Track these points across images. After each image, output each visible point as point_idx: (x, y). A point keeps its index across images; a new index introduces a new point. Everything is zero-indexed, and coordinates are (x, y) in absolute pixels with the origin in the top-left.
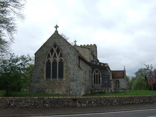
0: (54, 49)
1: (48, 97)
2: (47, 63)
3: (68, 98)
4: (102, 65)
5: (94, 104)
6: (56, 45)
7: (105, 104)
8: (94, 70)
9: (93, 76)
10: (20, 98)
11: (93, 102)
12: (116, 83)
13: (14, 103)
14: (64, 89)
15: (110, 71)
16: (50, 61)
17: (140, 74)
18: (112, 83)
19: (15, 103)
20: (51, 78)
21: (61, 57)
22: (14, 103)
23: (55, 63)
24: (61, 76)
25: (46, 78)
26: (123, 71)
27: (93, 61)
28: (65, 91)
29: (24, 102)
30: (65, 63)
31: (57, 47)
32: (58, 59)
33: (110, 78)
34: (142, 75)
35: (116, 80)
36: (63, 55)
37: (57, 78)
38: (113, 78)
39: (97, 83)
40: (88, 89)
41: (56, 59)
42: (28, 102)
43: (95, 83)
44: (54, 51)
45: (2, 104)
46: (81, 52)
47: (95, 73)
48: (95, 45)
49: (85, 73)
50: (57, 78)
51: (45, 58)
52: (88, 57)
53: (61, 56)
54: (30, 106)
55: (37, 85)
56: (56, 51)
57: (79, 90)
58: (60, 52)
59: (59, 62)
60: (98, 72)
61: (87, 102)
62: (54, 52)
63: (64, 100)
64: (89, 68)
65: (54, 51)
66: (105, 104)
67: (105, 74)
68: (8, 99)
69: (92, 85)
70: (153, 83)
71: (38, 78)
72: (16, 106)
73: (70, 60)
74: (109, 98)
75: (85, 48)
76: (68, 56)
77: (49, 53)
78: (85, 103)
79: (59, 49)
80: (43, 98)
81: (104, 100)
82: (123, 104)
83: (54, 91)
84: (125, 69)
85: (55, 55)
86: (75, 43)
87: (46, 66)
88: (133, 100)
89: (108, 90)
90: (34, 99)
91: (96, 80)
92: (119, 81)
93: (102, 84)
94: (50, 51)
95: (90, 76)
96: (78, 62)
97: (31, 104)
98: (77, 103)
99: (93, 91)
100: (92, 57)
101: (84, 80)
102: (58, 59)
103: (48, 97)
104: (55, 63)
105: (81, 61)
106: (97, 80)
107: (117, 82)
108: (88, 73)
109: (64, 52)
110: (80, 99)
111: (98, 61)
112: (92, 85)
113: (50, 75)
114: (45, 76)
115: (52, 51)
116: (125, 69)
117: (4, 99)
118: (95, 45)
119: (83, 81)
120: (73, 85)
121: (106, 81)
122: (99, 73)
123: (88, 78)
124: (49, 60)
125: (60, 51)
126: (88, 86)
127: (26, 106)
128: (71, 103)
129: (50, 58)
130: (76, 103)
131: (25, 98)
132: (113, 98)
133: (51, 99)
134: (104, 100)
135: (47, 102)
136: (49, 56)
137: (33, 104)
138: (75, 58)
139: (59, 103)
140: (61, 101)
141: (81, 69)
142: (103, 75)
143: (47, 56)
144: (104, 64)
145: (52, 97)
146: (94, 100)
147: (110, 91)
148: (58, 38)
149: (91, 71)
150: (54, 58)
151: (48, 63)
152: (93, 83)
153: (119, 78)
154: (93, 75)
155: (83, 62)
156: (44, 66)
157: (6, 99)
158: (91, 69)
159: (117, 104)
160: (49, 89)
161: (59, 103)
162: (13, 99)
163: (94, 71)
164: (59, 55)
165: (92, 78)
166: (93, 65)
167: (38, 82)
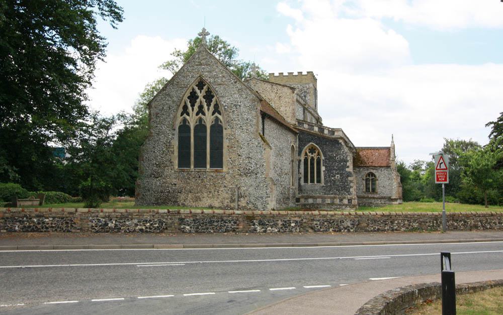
0: (198, 91)
1: (188, 210)
2: (180, 127)
3: (234, 213)
4: (44, 294)
5: (297, 229)
6: (202, 82)
7: (322, 230)
8: (305, 145)
9: (303, 161)
10: (127, 212)
11: (293, 225)
12: (367, 180)
13: (114, 222)
14: (225, 195)
15: (346, 149)
16: (187, 124)
17: (447, 157)
18: (351, 182)
19: (116, 221)
20: (192, 167)
21: (217, 114)
22: (114, 222)
23: (201, 127)
24: (217, 162)
25: (180, 165)
26: (388, 149)
28: (227, 199)
29: (136, 221)
30: (226, 129)
31: (205, 88)
32: (209, 119)
33: (348, 167)
34: (453, 161)
35: (367, 172)
36: (221, 109)
37: (208, 166)
38: (355, 166)
39: (312, 181)
40: (286, 196)
42: (146, 221)
43: (306, 181)
44: (198, 97)
45: (90, 223)
46: (269, 94)
47: (306, 154)
48: (311, 74)
49: (279, 155)
50: (208, 166)
52: (288, 110)
53: (217, 110)
54: (150, 229)
56: (204, 97)
57: (262, 198)
58: (214, 100)
59: (212, 127)
61: (280, 223)
62: (198, 100)
63: (225, 218)
64: (291, 140)
66: (322, 230)
67: (335, 157)
68: (101, 214)
69: (300, 185)
70: (446, 182)
71: (158, 166)
72: (120, 228)
73: (239, 120)
74: (332, 216)
75: (280, 85)
76: (233, 111)
77: (185, 103)
78: (276, 225)
79: (211, 92)
80: (179, 213)
81: (319, 221)
82: (366, 231)
83: (200, 199)
84: (393, 142)
85: (201, 110)
87: (179, 135)
88: (392, 222)
89: (341, 200)
90: (158, 213)
91: (310, 171)
92: (375, 176)
93: (326, 182)
94: (189, 98)
95: (293, 161)
96: (261, 126)
97: (151, 224)
98: (257, 226)
99: (302, 201)
100: (301, 110)
101: (276, 171)
102: (209, 119)
103: (188, 210)
104: (201, 127)
105: (268, 123)
106: (312, 173)
107: (371, 180)
109: (225, 101)
110: (264, 216)
111: (318, 120)
112: (300, 185)
114: (176, 162)
115: (193, 97)
116: (393, 142)
117: (93, 213)
119: (272, 174)
120: (247, 184)
121: (338, 177)
122: (319, 154)
123: (287, 167)
124: (185, 120)
125: (213, 97)
126: (289, 189)
128: (242, 224)
129: (188, 114)
130: (254, 225)
131: (139, 212)
132: (343, 216)
133: (195, 215)
134: (319, 221)
135: (188, 221)
136: (185, 110)
137: (156, 224)
138: (254, 117)
139: (215, 224)
140: (220, 220)
141: (268, 144)
142: (329, 159)
143: (181, 110)
144: (332, 131)
145: (199, 211)
146: (297, 219)
147: (345, 201)
148: (209, 65)
149: (296, 149)
150: (197, 114)
151: (184, 128)
152: (302, 180)
153: (375, 167)
154: (302, 158)
155: (274, 126)
156: (173, 135)
157: (97, 214)
159: (352, 230)
160: (188, 194)
161: (215, 224)
162: (112, 213)
163: (306, 149)
164: (212, 108)
166: (302, 132)
167: (157, 176)
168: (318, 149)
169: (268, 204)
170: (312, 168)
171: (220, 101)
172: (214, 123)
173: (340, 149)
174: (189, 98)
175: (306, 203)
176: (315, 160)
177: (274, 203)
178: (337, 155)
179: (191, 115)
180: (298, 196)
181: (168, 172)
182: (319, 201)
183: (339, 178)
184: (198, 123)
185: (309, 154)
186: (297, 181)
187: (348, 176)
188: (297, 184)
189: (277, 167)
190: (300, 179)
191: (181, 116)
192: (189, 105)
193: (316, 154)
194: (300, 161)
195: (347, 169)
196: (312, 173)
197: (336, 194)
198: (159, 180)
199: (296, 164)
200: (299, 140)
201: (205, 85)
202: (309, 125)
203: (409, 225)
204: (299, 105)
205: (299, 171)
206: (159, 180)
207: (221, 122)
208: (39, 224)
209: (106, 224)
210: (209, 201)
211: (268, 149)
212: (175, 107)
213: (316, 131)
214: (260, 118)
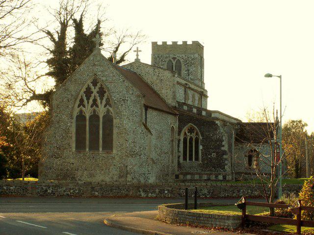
0: (92, 87)
2: (77, 117)
8: (185, 125)
11: (166, 192)
18: (226, 159)
24: (108, 145)
25: (77, 147)
27: (181, 105)
32: (101, 111)
33: (223, 146)
39: (191, 159)
41: (96, 109)
43: (185, 159)
51: (74, 107)
55: (57, 162)
56: (98, 92)
57: (144, 174)
58: (106, 95)
59: (104, 117)
60: (188, 132)
61: (157, 191)
62: (93, 95)
64: (172, 122)
65: (92, 92)
68: (44, 184)
69: (179, 163)
76: (122, 105)
78: (154, 192)
79: (103, 88)
85: (95, 102)
86: (137, 55)
89: (217, 176)
91: (189, 149)
93: (203, 160)
95: (172, 141)
96: (144, 117)
99: (181, 177)
102: (101, 111)
104: (95, 117)
106: (191, 151)
108: (167, 135)
109: (115, 97)
113: (85, 143)
114: (74, 145)
115: (88, 92)
118: (198, 47)
122: (197, 134)
123: (167, 147)
124: (81, 111)
125: (105, 92)
126: (168, 167)
127: (68, 194)
129: (84, 106)
130: (140, 192)
141: (150, 131)
143: (78, 102)
147: (221, 177)
151: (81, 117)
152: (182, 158)
154: (182, 138)
155: (155, 113)
156: (72, 123)
158: (177, 123)
161: (115, 191)
163: (185, 129)
164: (104, 102)
165: (178, 146)
167: (56, 156)
168: (196, 129)
169: (149, 179)
170: (191, 147)
171: (111, 96)
172: (105, 114)
173: (216, 129)
174: (84, 92)
175: (185, 178)
176: (194, 140)
177: (154, 178)
178: (213, 135)
179: (86, 107)
180: (177, 173)
181: (66, 153)
182: (197, 177)
183: (215, 156)
184: (92, 114)
185: (188, 134)
186: (177, 160)
187: (223, 154)
188: (177, 162)
189: (157, 148)
190: (179, 157)
191: (78, 107)
192: (85, 98)
193: (195, 134)
194: (179, 141)
195: (223, 148)
196: (191, 151)
197: (211, 170)
198: (60, 160)
199: (175, 144)
200: (179, 120)
201: (98, 83)
202: (188, 107)
203: (252, 193)
204: (180, 87)
205: (178, 149)
206: (60, 160)
207: (111, 113)
208: (7, 190)
209: (46, 191)
210: (101, 177)
211: (149, 136)
212: (73, 100)
213: (194, 113)
214: (144, 110)
